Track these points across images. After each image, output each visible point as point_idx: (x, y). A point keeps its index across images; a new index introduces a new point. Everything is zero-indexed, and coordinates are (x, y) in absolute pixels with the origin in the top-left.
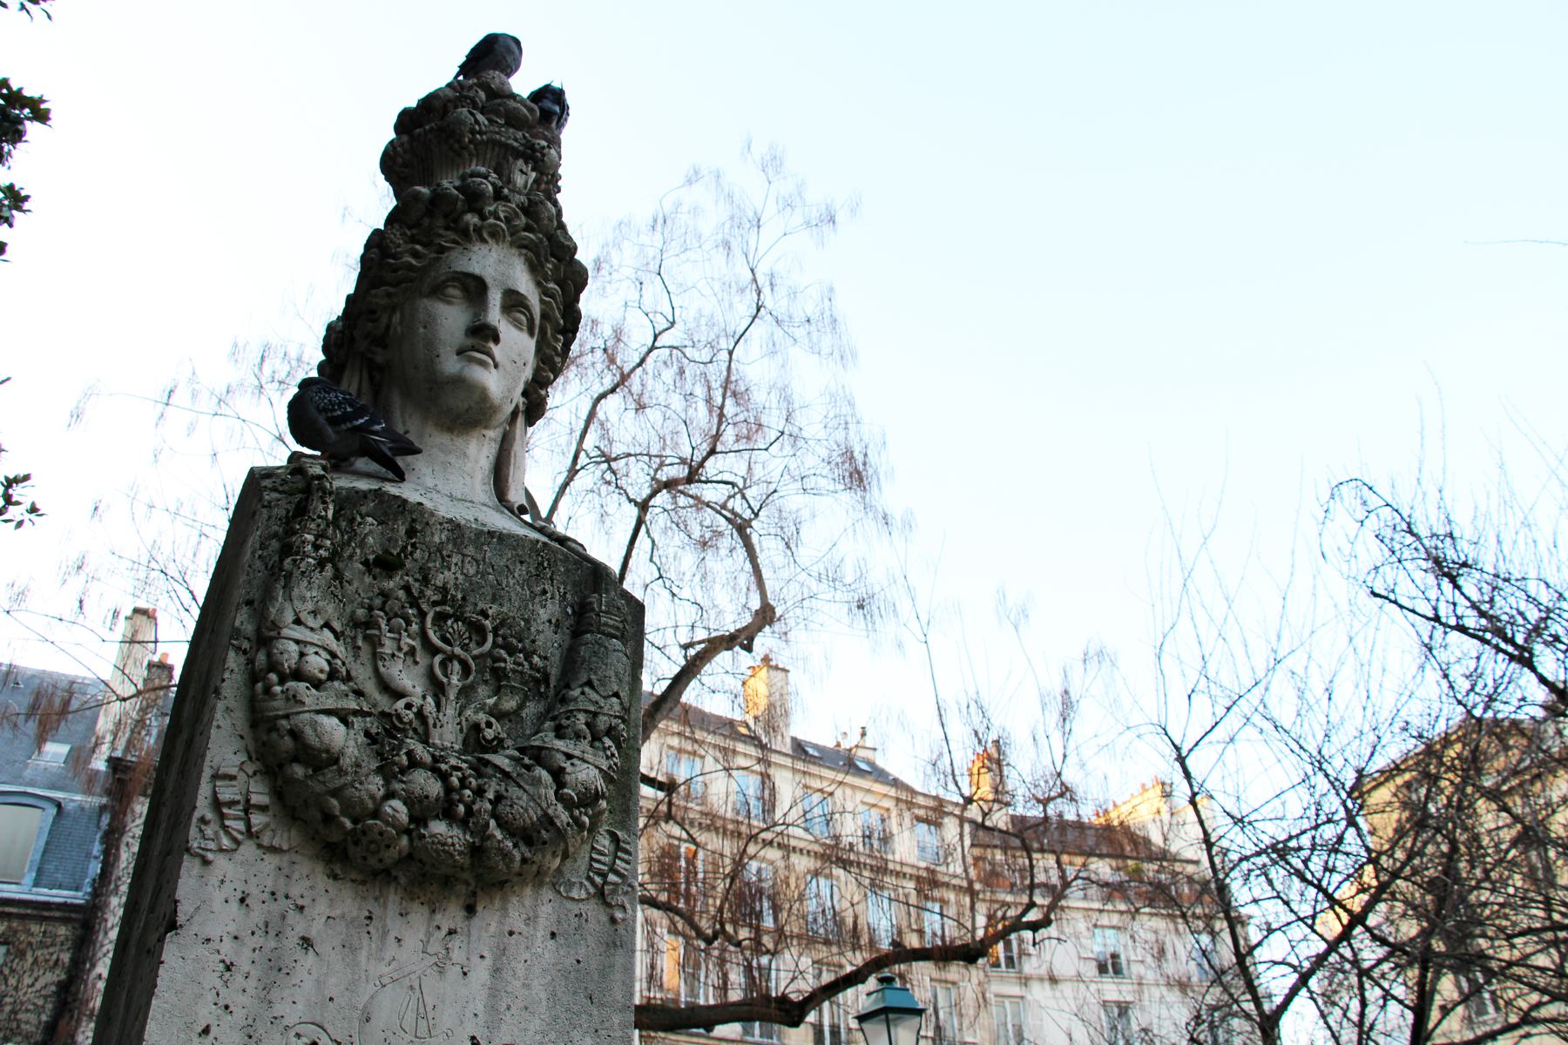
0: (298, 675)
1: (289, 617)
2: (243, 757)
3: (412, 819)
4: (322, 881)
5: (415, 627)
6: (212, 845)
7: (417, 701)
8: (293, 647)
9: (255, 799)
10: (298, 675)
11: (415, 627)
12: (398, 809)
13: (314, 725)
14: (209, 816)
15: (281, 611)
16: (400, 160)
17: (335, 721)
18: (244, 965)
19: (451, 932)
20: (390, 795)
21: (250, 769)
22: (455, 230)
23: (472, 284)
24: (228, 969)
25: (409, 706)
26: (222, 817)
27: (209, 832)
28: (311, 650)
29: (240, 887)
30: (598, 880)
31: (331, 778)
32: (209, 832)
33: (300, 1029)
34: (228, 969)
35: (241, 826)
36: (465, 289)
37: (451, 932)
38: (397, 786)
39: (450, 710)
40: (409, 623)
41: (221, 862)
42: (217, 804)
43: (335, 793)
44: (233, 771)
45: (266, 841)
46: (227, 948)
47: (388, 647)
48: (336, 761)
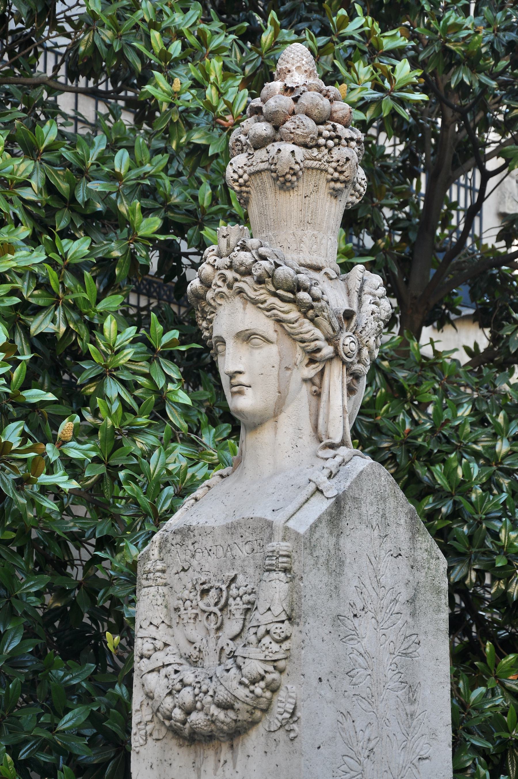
4: (176, 749)
37: (225, 762)
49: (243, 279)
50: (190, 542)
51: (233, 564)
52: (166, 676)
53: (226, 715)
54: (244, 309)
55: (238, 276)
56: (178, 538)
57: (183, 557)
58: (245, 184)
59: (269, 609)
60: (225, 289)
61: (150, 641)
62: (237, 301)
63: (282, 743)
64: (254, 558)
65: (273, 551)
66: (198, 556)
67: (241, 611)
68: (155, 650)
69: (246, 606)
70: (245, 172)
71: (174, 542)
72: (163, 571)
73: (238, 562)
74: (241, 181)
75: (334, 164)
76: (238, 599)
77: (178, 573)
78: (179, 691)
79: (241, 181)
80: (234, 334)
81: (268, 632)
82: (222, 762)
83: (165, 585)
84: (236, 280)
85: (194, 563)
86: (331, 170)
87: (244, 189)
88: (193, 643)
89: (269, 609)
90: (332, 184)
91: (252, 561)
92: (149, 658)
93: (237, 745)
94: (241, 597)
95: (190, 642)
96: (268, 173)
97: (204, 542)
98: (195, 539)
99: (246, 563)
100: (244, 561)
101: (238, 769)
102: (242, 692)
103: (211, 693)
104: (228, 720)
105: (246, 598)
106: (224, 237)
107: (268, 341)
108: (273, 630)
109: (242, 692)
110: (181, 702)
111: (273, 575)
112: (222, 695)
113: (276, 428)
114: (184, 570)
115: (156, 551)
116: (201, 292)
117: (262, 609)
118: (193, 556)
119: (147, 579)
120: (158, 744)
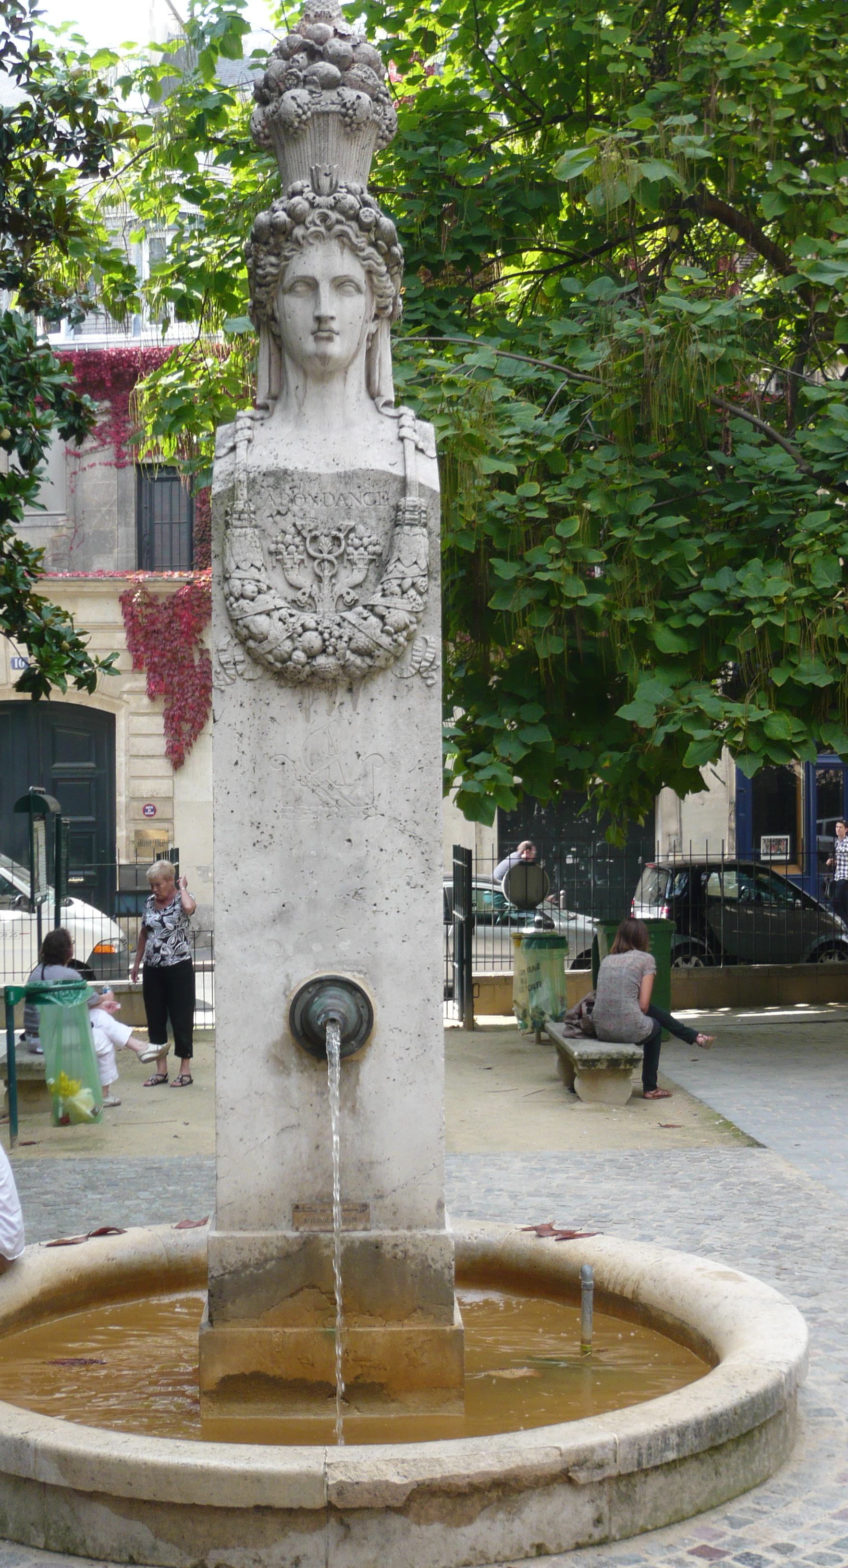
0: (243, 596)
1: (233, 566)
2: (229, 638)
3: (308, 657)
4: (275, 690)
5: (301, 548)
6: (222, 683)
7: (307, 590)
8: (238, 583)
9: (238, 658)
10: (243, 596)
11: (301, 548)
12: (300, 656)
13: (253, 622)
14: (219, 670)
15: (229, 563)
16: (262, 135)
17: (264, 617)
18: (246, 733)
19: (341, 704)
20: (295, 649)
21: (233, 643)
22: (291, 241)
23: (311, 282)
24: (241, 735)
25: (304, 594)
26: (225, 669)
27: (221, 677)
28: (246, 582)
29: (239, 699)
30: (417, 666)
31: (266, 646)
32: (221, 677)
33: (277, 757)
34: (241, 735)
35: (233, 672)
36: (308, 284)
37: (341, 704)
38: (297, 644)
39: (326, 589)
40: (297, 547)
41: (228, 689)
42: (222, 664)
43: (270, 652)
44: (225, 647)
45: (246, 676)
46: (239, 728)
47: (289, 564)
48: (266, 638)
49: (350, 223)
50: (287, 486)
51: (348, 514)
52: (280, 620)
53: (363, 661)
54: (342, 253)
55: (343, 219)
56: (271, 480)
57: (278, 501)
58: (305, 123)
59: (416, 563)
60: (322, 229)
61: (254, 583)
62: (335, 245)
63: (415, 689)
64: (375, 510)
65: (415, 506)
66: (298, 501)
67: (366, 561)
68: (259, 592)
69: (370, 557)
70: (309, 109)
71: (265, 484)
72: (254, 513)
73: (355, 513)
74: (304, 117)
75: (387, 122)
76: (362, 549)
77: (271, 516)
78: (300, 636)
79: (304, 117)
80: (331, 277)
81: (413, 585)
82: (338, 704)
83: (256, 527)
84: (339, 222)
85: (295, 508)
86: (384, 127)
87: (303, 126)
88: (300, 589)
89: (416, 563)
90: (380, 141)
91: (374, 514)
92: (253, 599)
93: (358, 689)
94: (366, 548)
95: (291, 586)
96: (336, 117)
97: (308, 489)
98: (294, 484)
99: (366, 514)
100: (363, 512)
101: (359, 710)
102: (385, 640)
103: (346, 639)
104: (364, 665)
105: (371, 548)
106: (326, 175)
107: (359, 290)
108: (419, 583)
109: (385, 640)
110: (306, 645)
111: (417, 530)
112: (361, 641)
113: (345, 379)
114: (279, 513)
115: (245, 492)
116: (289, 227)
117: (407, 563)
118: (292, 501)
119: (239, 519)
120: (250, 684)
